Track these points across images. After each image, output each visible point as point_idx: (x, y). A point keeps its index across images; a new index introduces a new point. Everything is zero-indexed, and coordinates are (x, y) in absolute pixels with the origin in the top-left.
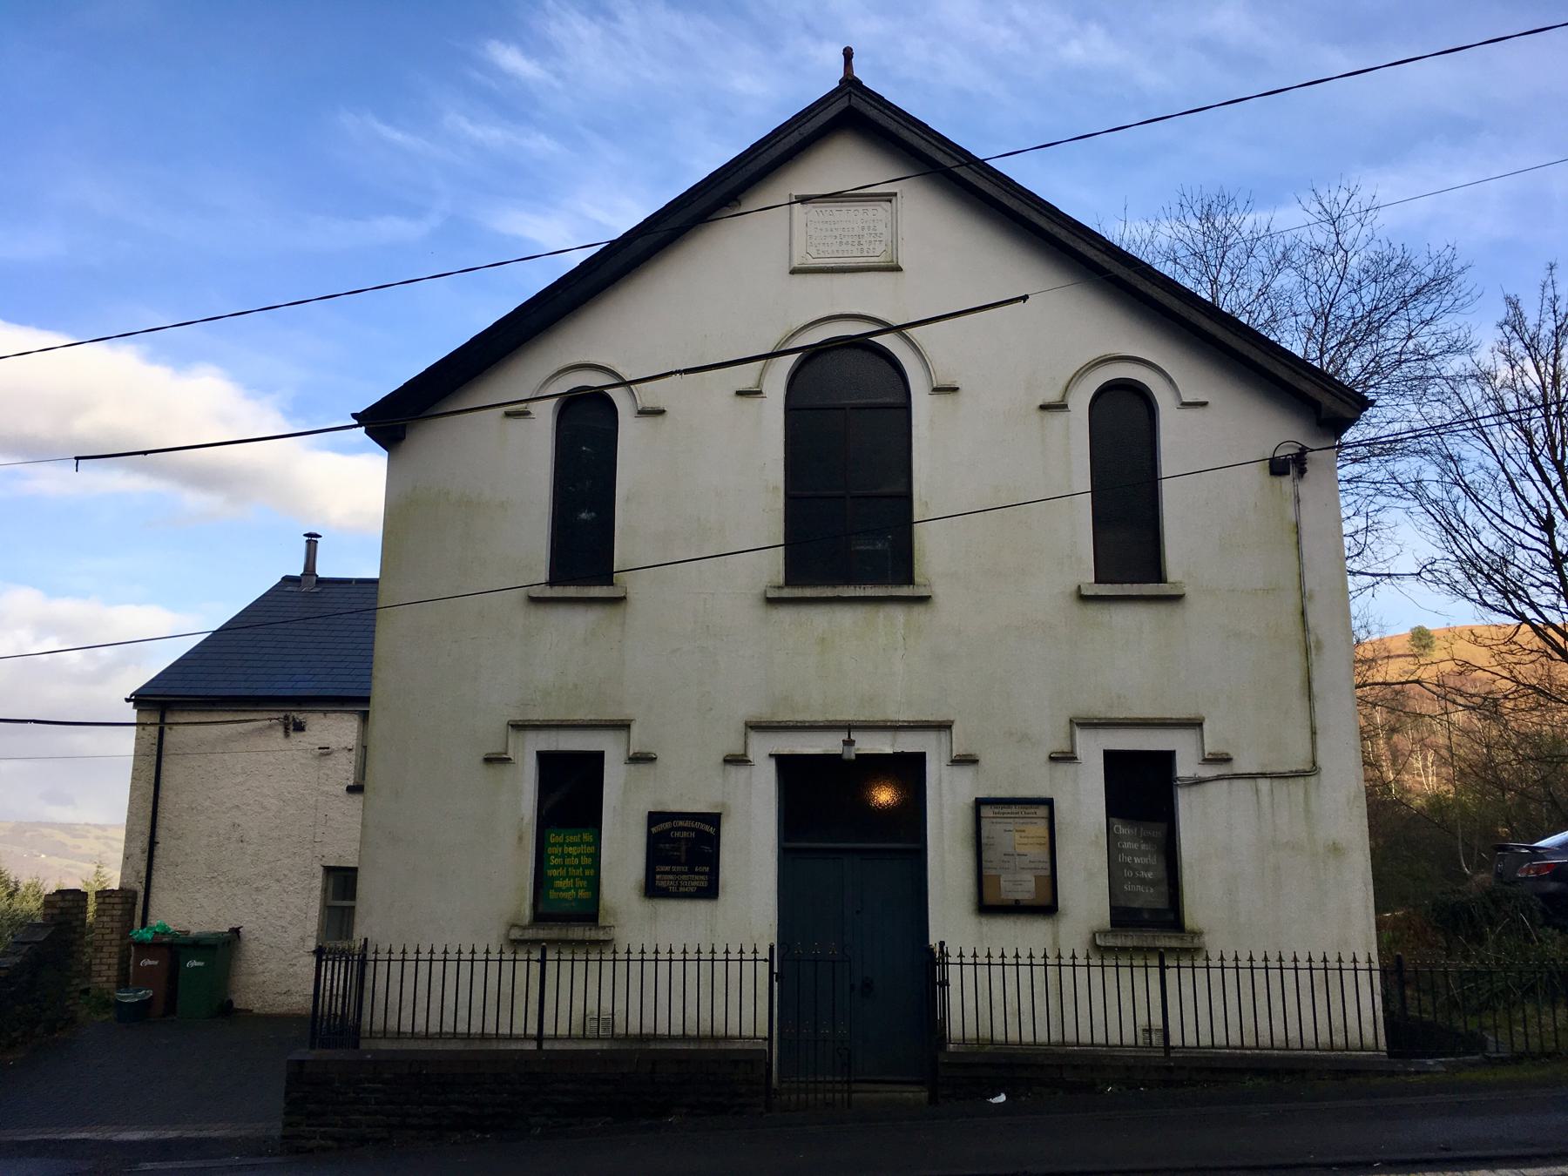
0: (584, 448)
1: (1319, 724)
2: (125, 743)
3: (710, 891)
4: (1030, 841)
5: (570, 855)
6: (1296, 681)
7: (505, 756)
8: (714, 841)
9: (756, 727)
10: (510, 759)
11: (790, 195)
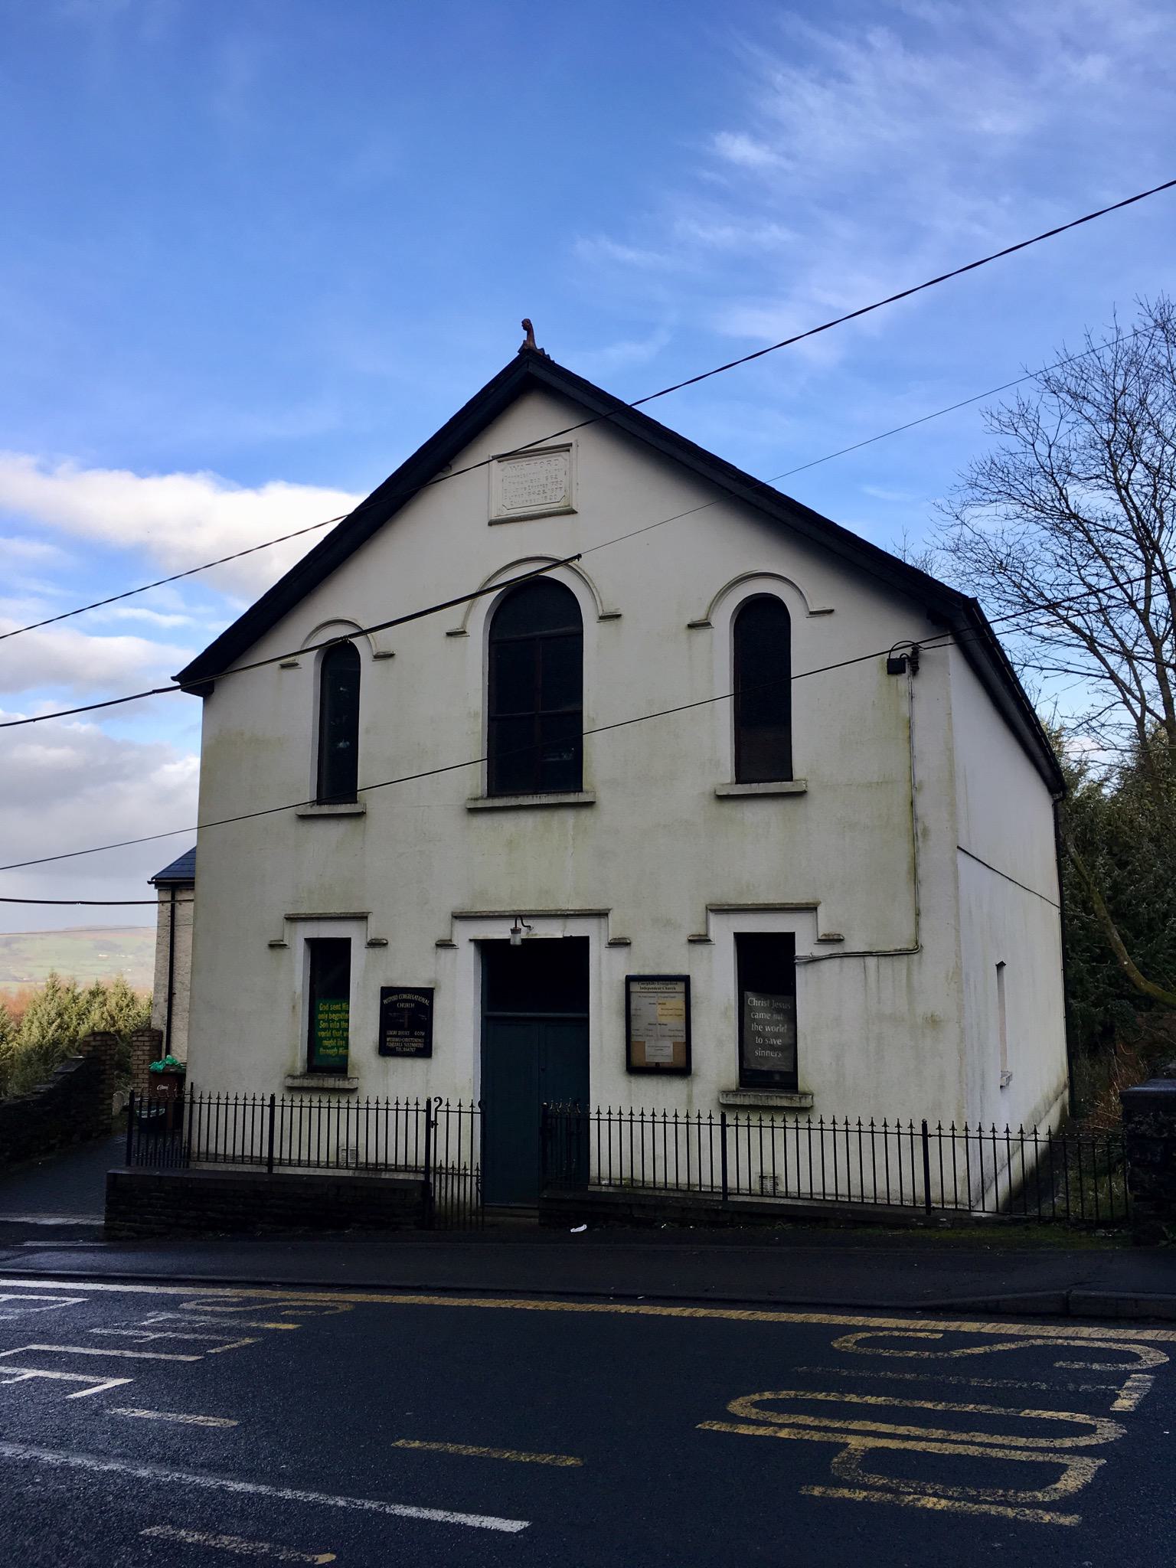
0: (341, 689)
1: (922, 905)
2: (150, 917)
3: (425, 1051)
4: (670, 1012)
5: (333, 1021)
6: (904, 867)
7: (282, 943)
8: (429, 1010)
9: (459, 917)
10: (286, 945)
11: (489, 456)
